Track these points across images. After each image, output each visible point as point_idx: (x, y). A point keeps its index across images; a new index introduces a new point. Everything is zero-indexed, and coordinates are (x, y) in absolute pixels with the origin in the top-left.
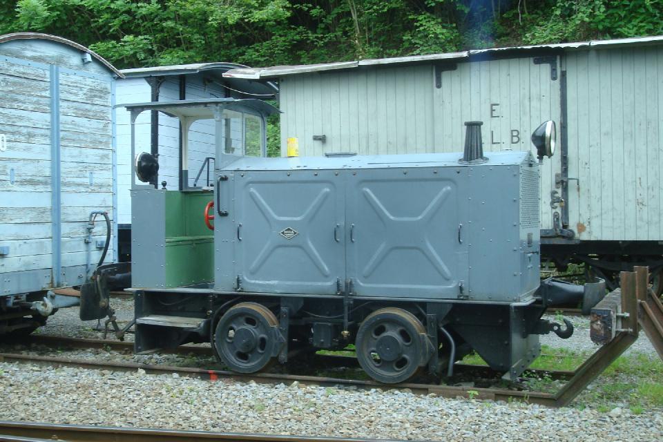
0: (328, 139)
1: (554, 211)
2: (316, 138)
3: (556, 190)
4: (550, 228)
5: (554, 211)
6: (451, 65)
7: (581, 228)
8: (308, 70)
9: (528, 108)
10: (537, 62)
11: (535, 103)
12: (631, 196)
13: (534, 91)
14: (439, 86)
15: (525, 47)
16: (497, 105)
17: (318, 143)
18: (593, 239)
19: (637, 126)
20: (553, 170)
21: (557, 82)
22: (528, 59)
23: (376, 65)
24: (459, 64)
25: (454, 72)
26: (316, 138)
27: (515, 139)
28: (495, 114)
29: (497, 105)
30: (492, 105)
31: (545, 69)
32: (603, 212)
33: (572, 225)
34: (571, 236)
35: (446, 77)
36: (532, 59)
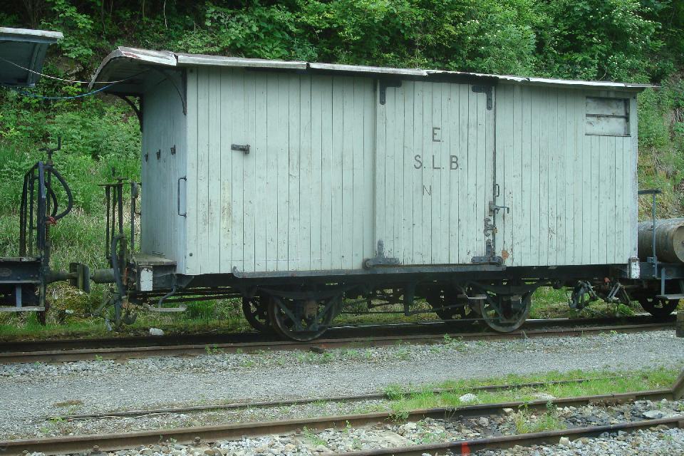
0: (251, 149)
1: (487, 238)
2: (234, 148)
3: (490, 218)
4: (627, 151)
5: (487, 238)
6: (396, 81)
7: (505, 254)
8: (245, 63)
9: (466, 135)
10: (475, 90)
11: (472, 130)
12: (545, 225)
13: (473, 118)
14: (383, 102)
15: (477, 75)
16: (439, 129)
17: (237, 154)
18: (515, 265)
19: (550, 160)
20: (487, 197)
21: (492, 111)
22: (457, 85)
23: (368, 72)
24: (403, 81)
25: (399, 90)
26: (234, 148)
27: (454, 165)
28: (436, 138)
29: (439, 129)
30: (434, 129)
31: (482, 98)
32: (515, 242)
33: (498, 253)
34: (499, 262)
35: (390, 92)
36: (470, 87)
